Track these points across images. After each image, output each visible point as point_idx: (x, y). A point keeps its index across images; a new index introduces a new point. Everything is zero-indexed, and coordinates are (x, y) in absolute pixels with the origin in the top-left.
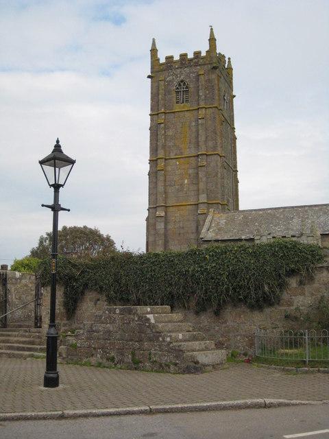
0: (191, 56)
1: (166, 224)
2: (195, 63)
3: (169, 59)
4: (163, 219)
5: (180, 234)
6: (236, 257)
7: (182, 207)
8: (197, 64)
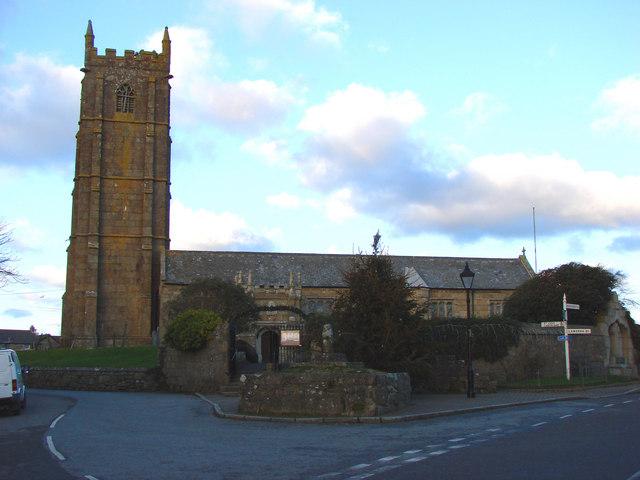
0: (120, 53)
1: (100, 256)
2: (145, 65)
4: (97, 252)
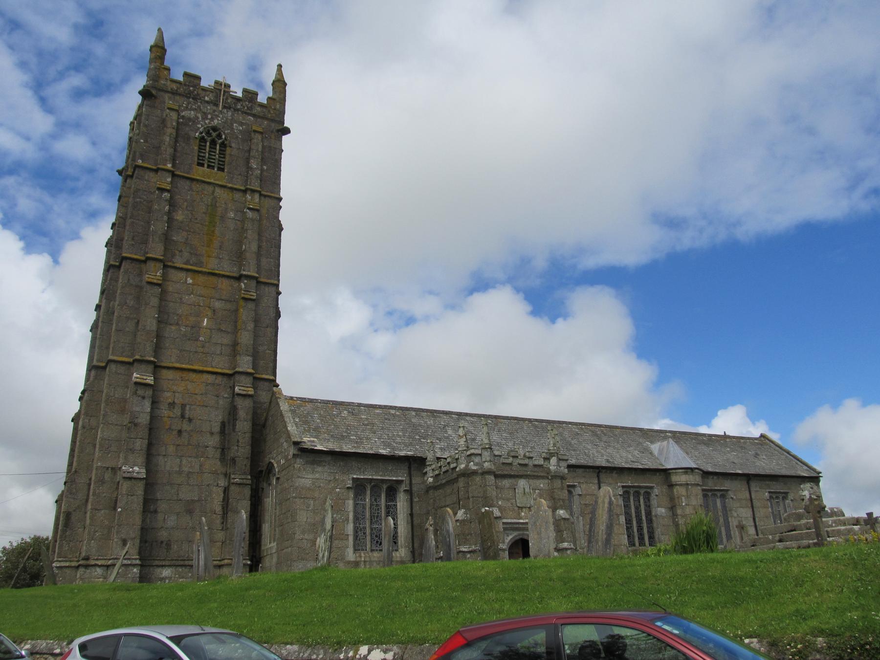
7: (193, 376)
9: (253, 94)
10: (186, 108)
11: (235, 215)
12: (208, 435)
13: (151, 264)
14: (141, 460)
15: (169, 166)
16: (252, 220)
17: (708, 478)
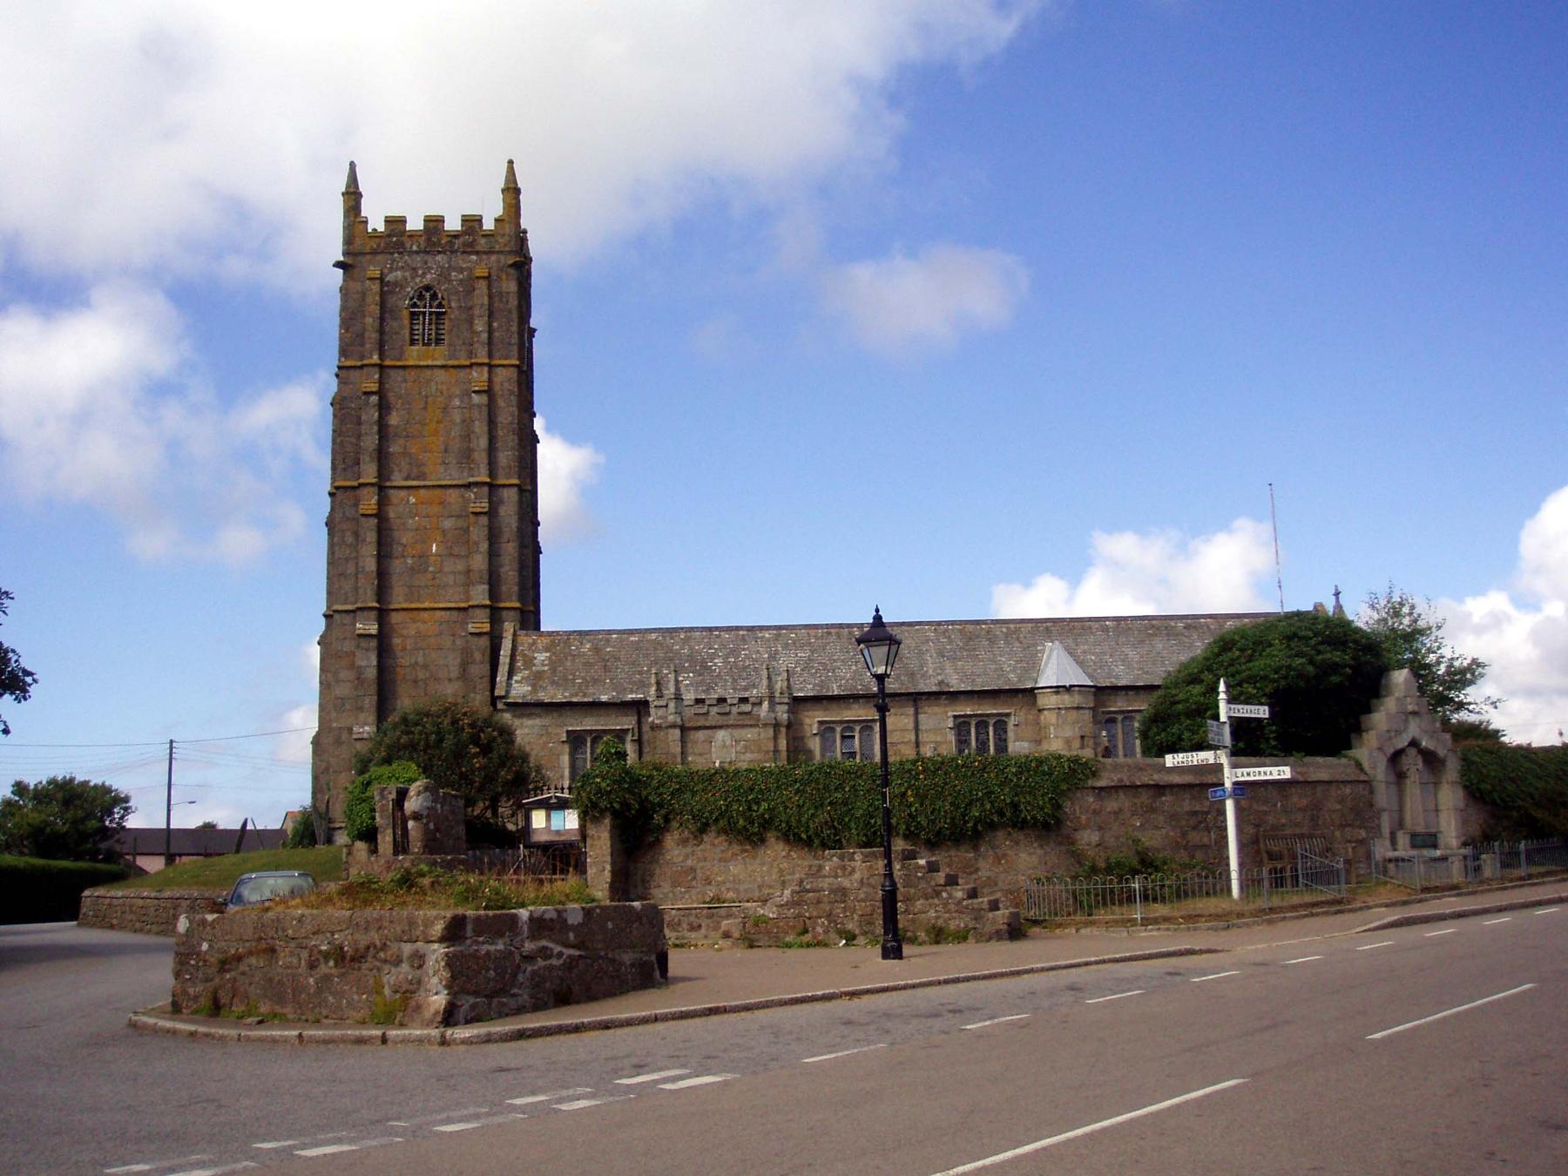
3: (395, 223)
4: (374, 643)
5: (415, 682)
6: (943, 788)
7: (425, 615)
8: (470, 249)
9: (436, 221)
10: (391, 270)
11: (462, 401)
12: (446, 682)
13: (365, 491)
14: (372, 718)
15: (375, 359)
16: (479, 406)
17: (1116, 695)
